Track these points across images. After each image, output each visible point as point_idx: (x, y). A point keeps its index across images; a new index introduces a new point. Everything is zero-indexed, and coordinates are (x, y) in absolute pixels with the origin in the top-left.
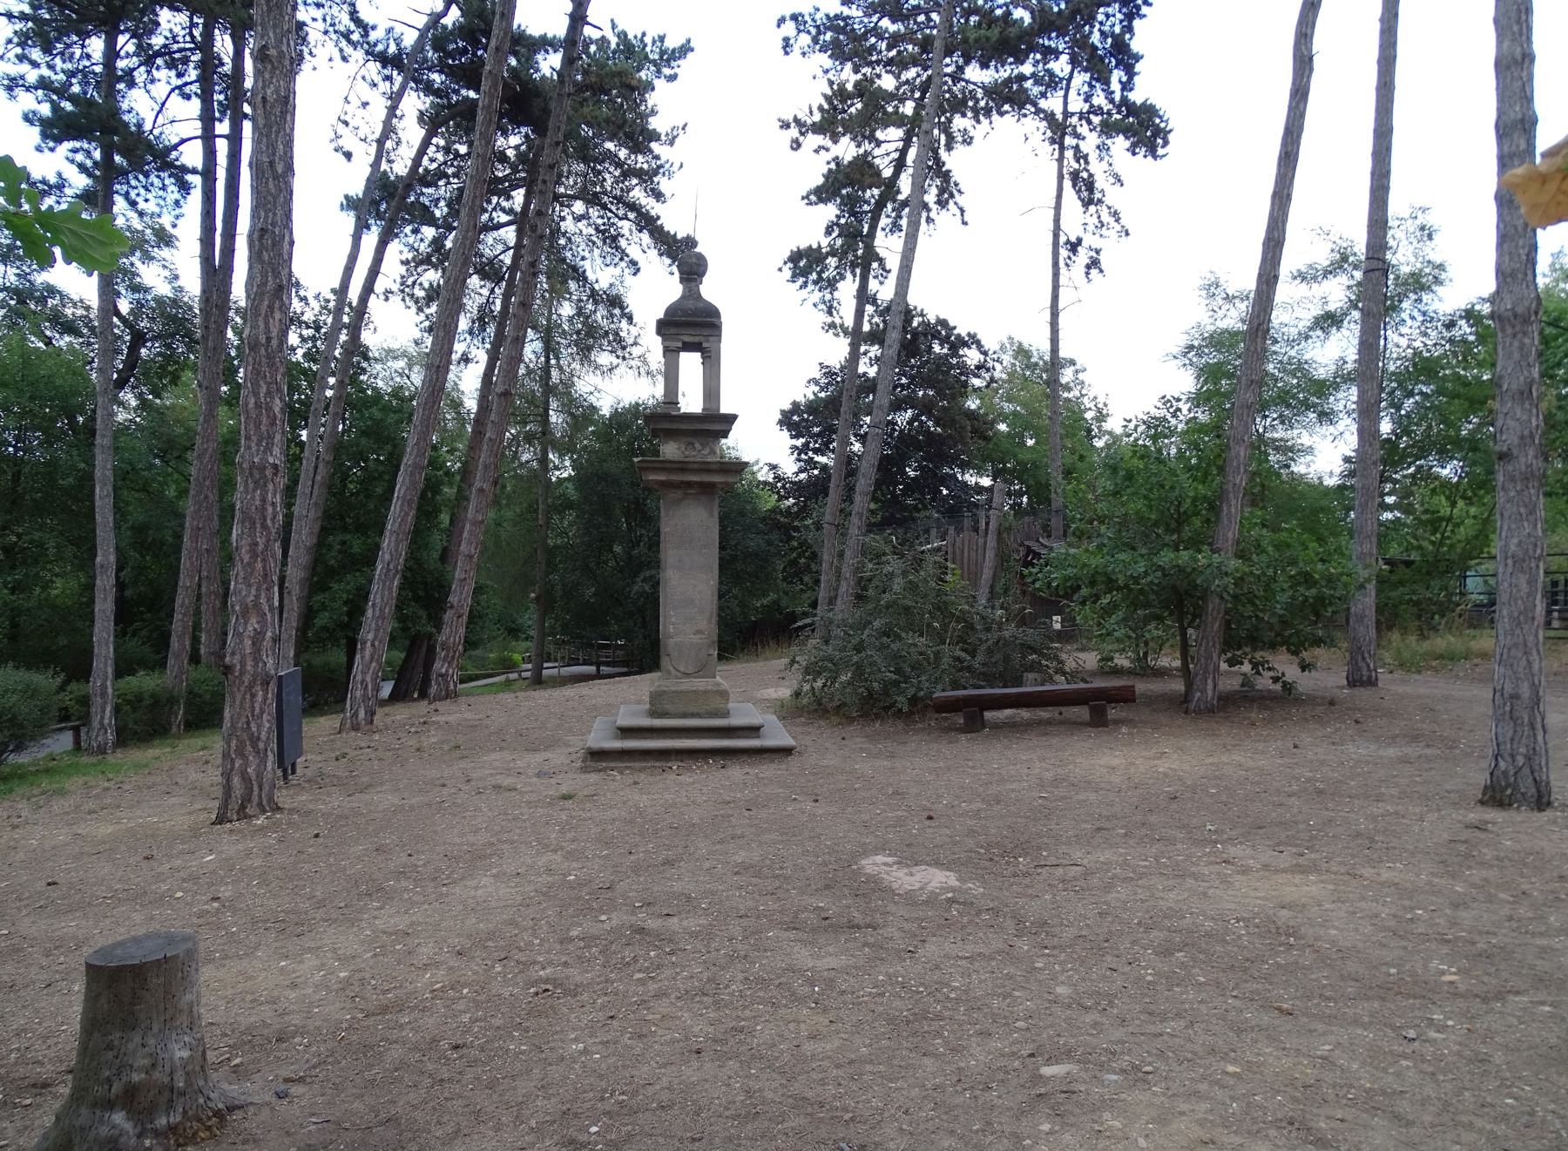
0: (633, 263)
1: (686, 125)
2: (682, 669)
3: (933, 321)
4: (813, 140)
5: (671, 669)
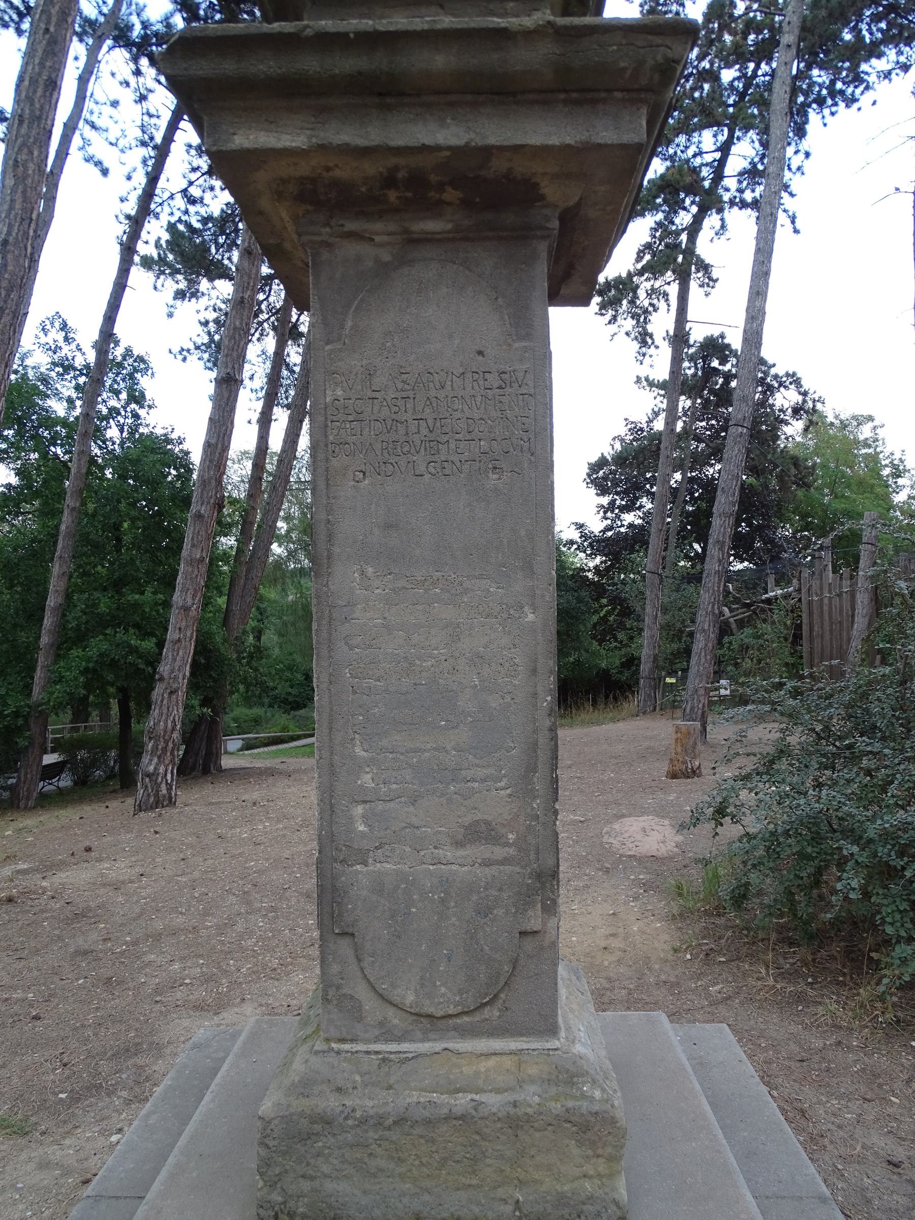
5: (362, 992)
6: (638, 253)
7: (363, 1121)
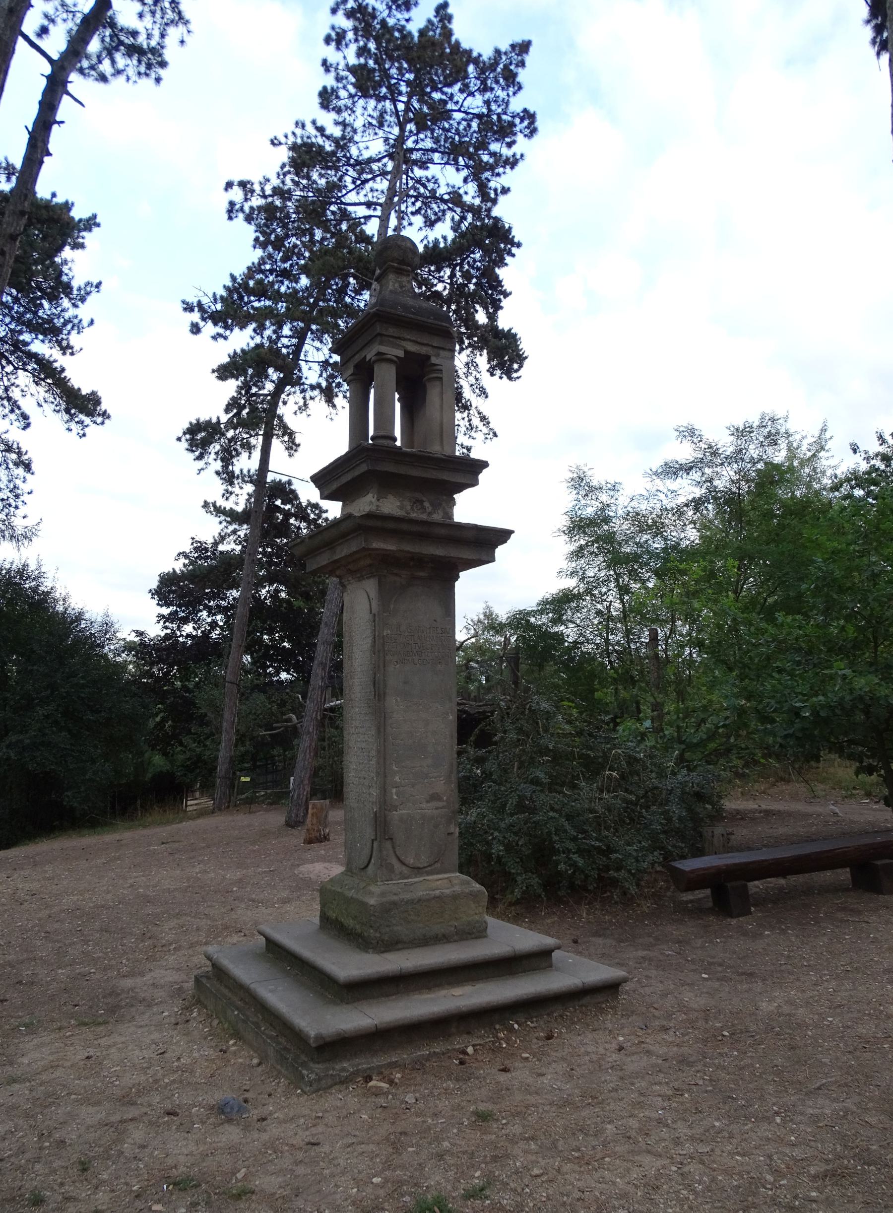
0: (25, 417)
1: (100, 283)
2: (411, 861)
3: (304, 505)
4: (209, 329)
5: (394, 861)
6: (227, 406)
7: (407, 903)
